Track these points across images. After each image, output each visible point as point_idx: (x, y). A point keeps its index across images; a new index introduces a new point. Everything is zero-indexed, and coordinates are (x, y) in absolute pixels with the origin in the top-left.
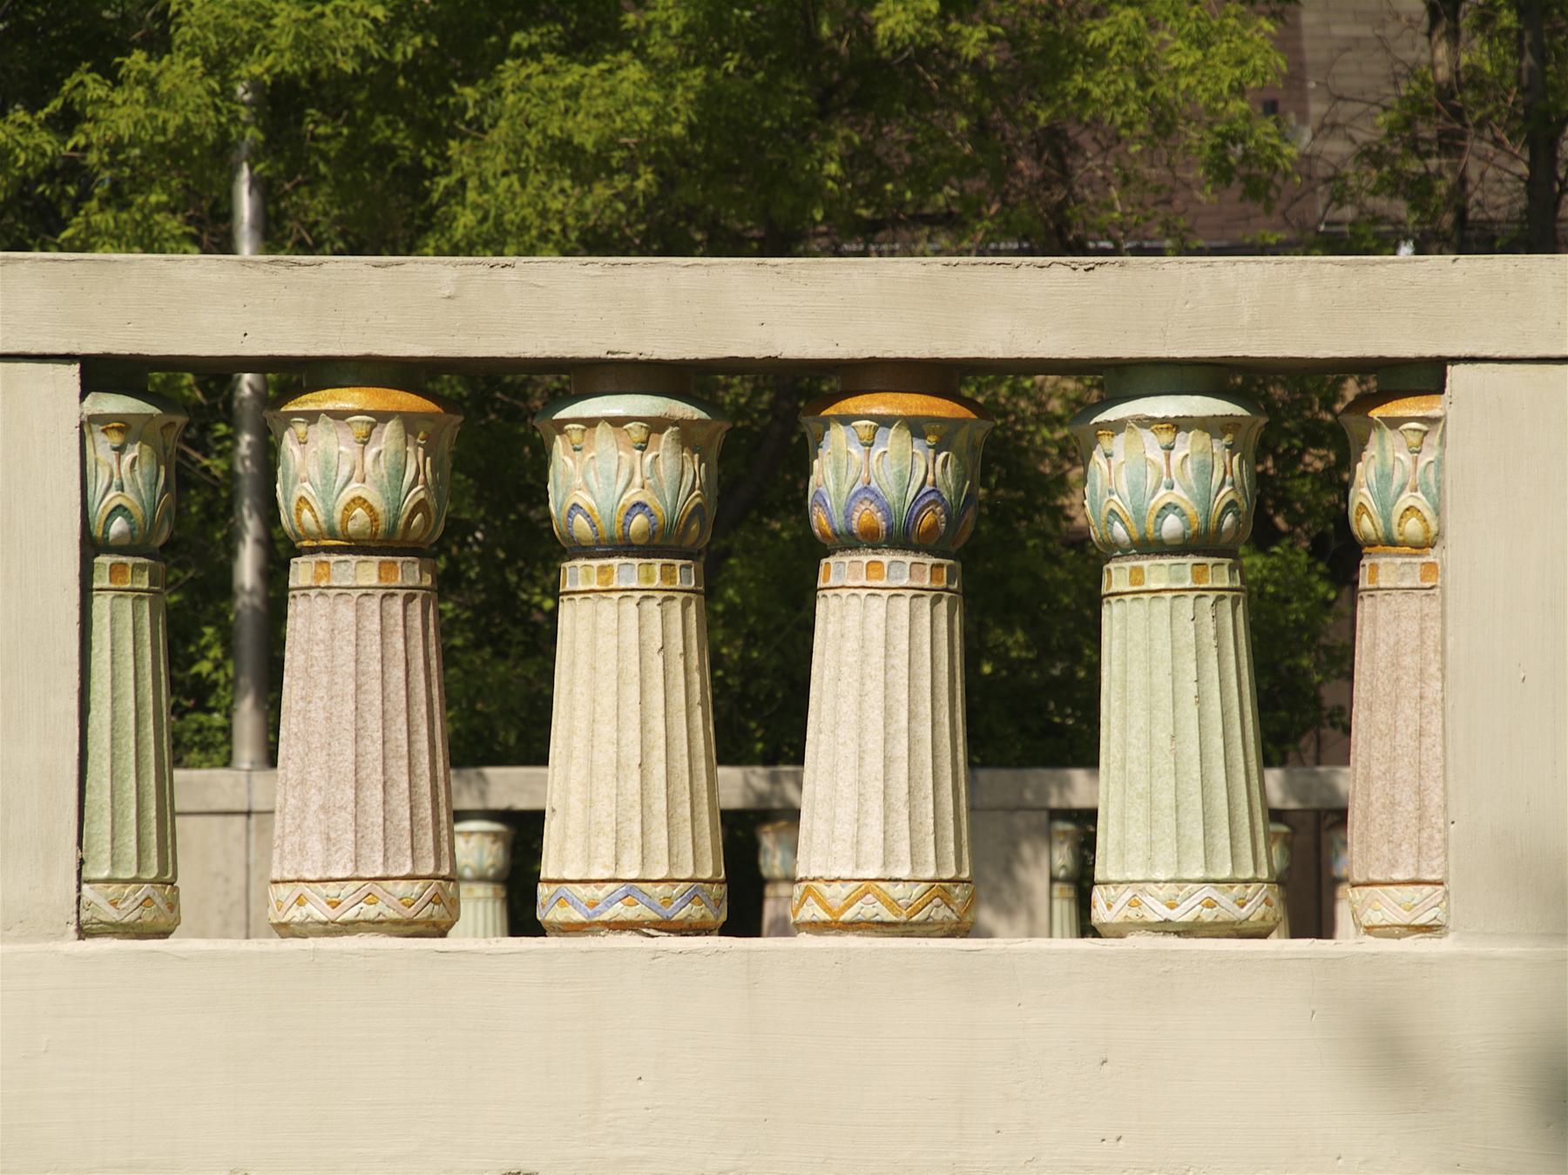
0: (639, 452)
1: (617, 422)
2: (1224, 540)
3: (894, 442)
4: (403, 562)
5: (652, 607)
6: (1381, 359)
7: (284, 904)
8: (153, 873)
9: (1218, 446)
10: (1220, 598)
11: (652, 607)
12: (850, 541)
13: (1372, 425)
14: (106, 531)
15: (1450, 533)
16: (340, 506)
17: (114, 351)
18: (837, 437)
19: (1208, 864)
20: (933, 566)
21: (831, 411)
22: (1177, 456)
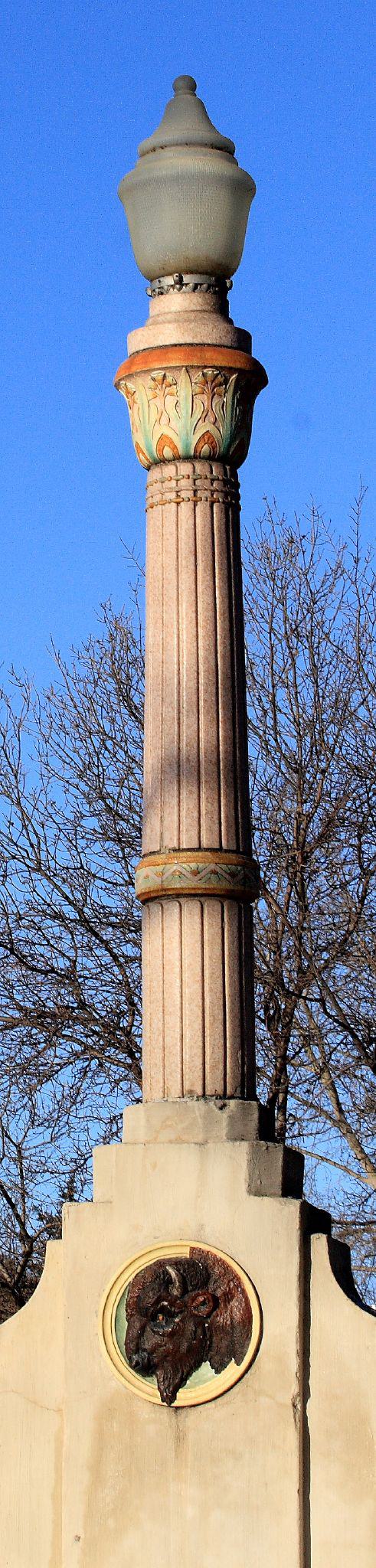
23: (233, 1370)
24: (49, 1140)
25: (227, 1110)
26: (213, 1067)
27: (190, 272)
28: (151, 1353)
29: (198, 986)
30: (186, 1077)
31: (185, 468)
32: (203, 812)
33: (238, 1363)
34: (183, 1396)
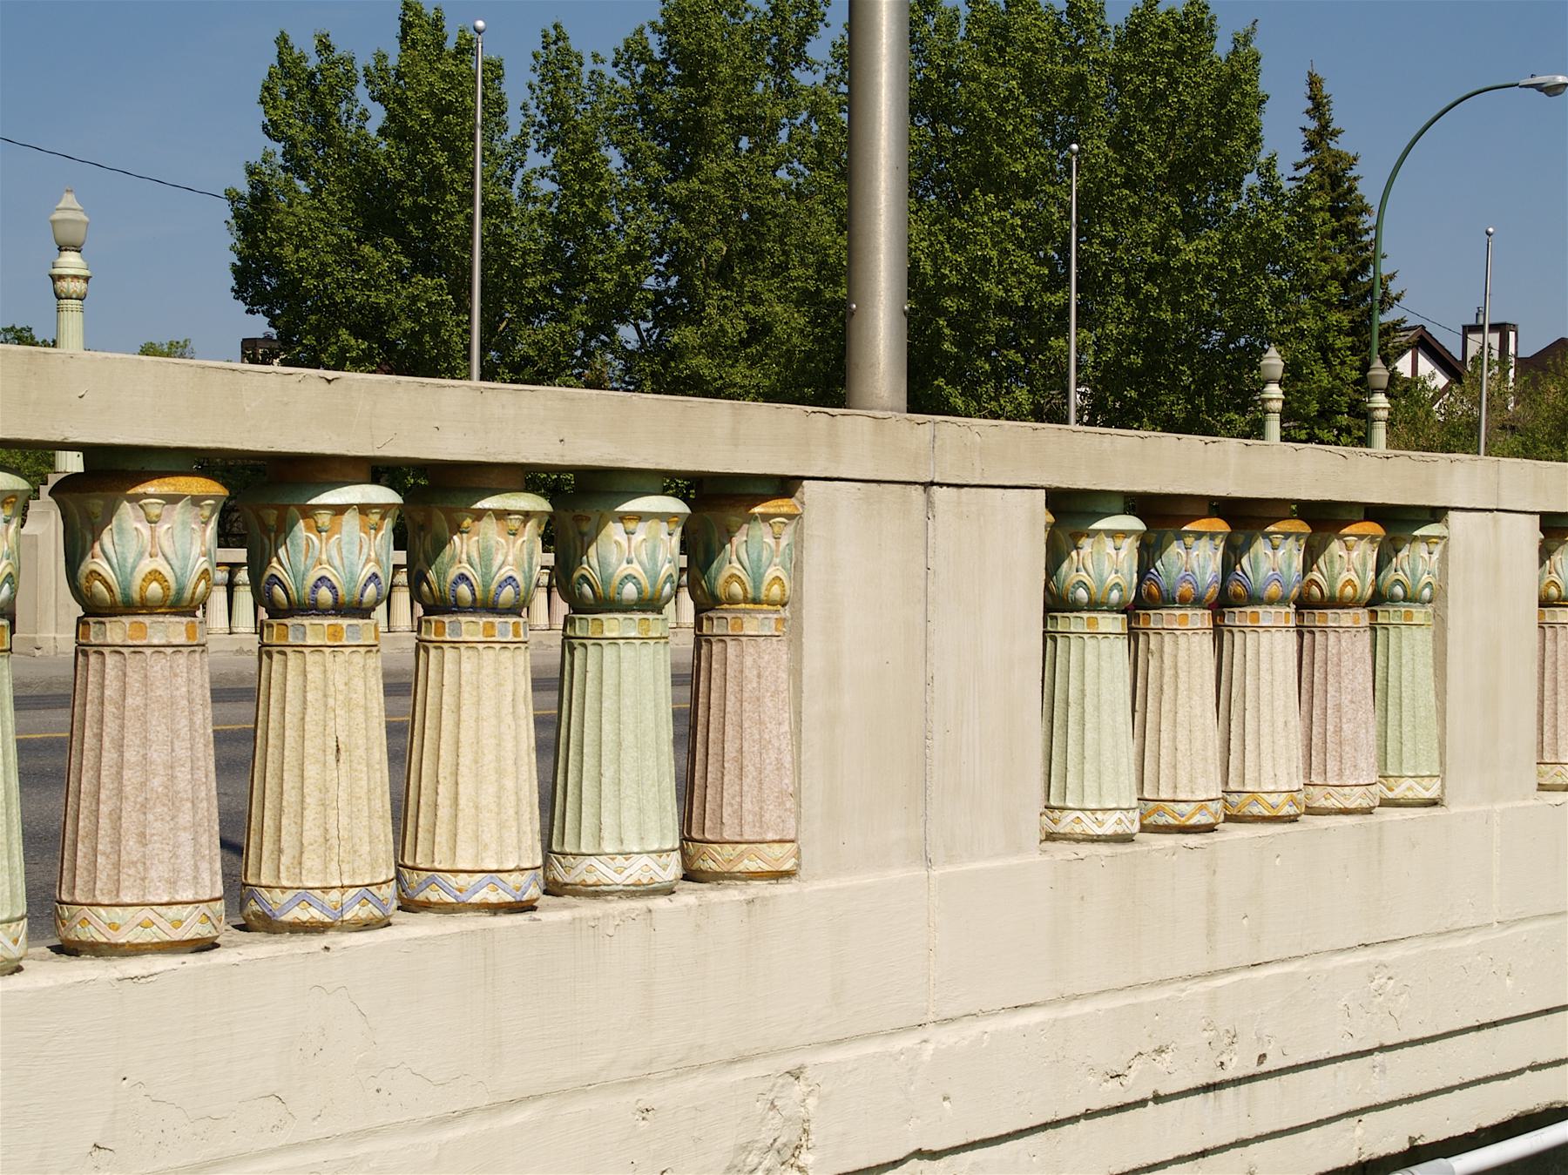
0: (373, 531)
1: (364, 509)
4: (131, 623)
6: (1085, 489)
14: (498, 594)
16: (498, 579)
17: (1313, 499)
18: (615, 531)
20: (188, 623)
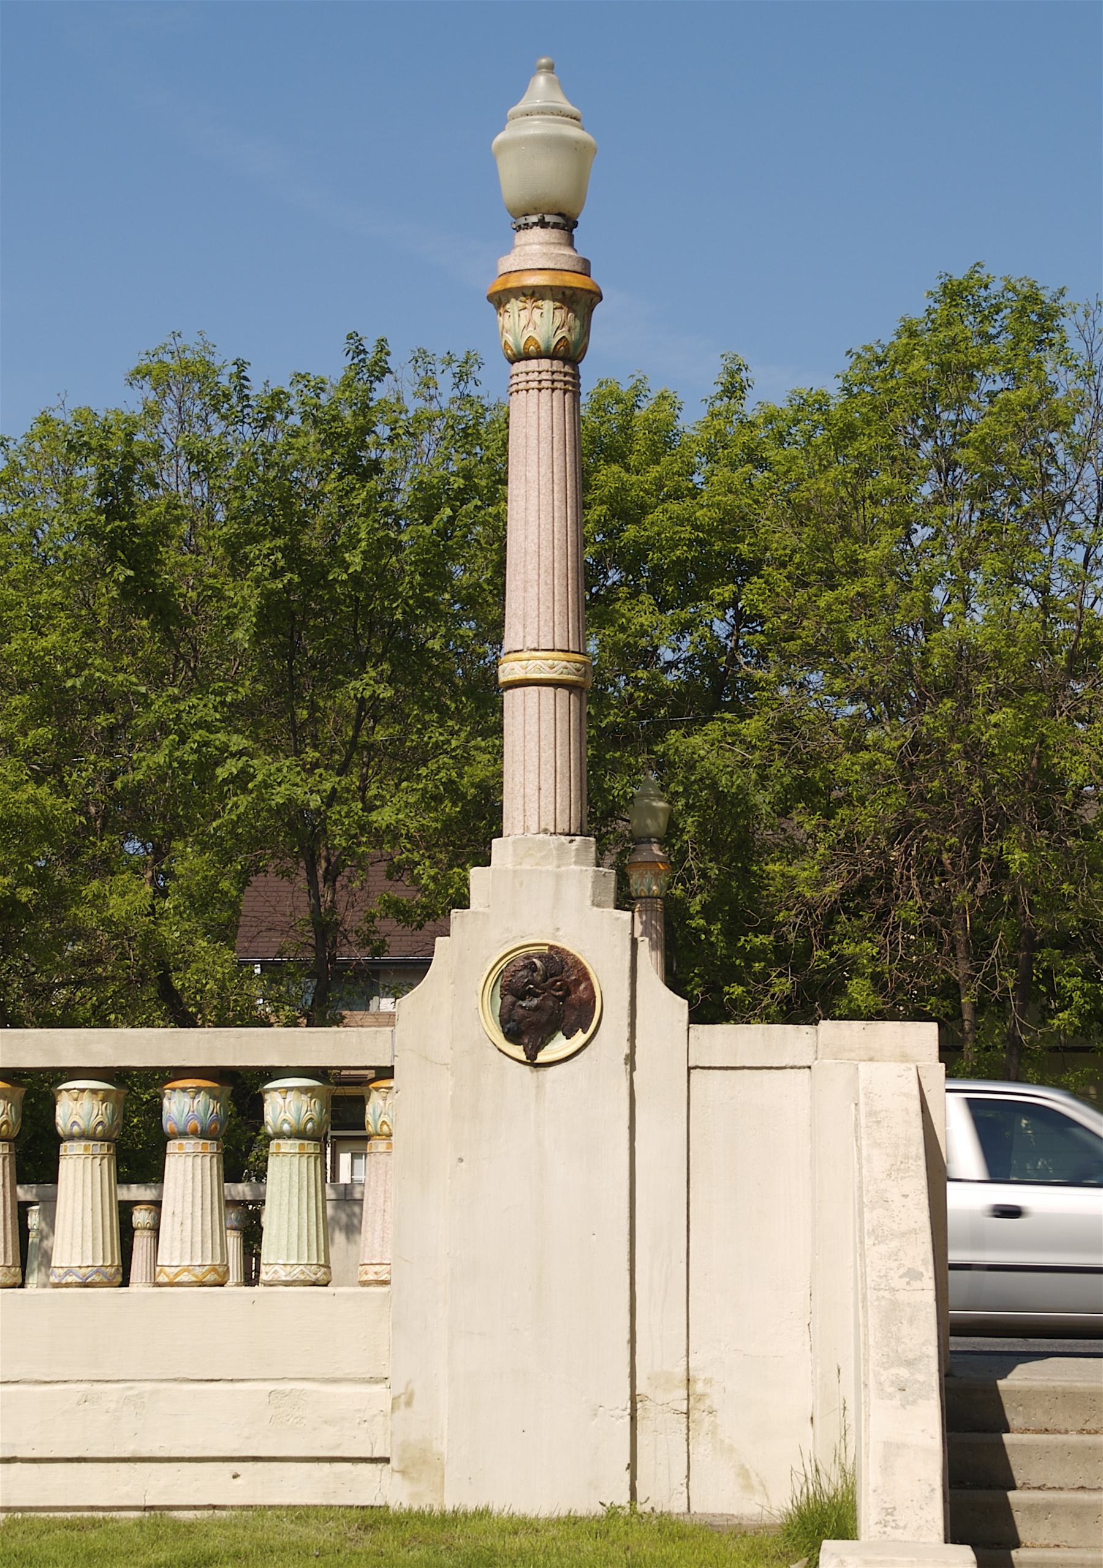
2: (309, 1133)
3: (86, 1100)
5: (199, 1160)
7: (162, 1279)
8: (322, 1262)
9: (305, 1098)
10: (102, 1159)
11: (199, 1160)
12: (72, 1137)
13: (370, 1092)
15: (393, 1132)
19: (298, 1258)
21: (60, 1087)
22: (287, 1101)
23: (580, 1038)
24: (630, 913)
25: (574, 843)
26: (563, 811)
27: (549, 213)
28: (519, 1023)
29: (551, 752)
30: (542, 818)
31: (545, 364)
32: (557, 622)
33: (585, 1033)
34: (541, 1057)
